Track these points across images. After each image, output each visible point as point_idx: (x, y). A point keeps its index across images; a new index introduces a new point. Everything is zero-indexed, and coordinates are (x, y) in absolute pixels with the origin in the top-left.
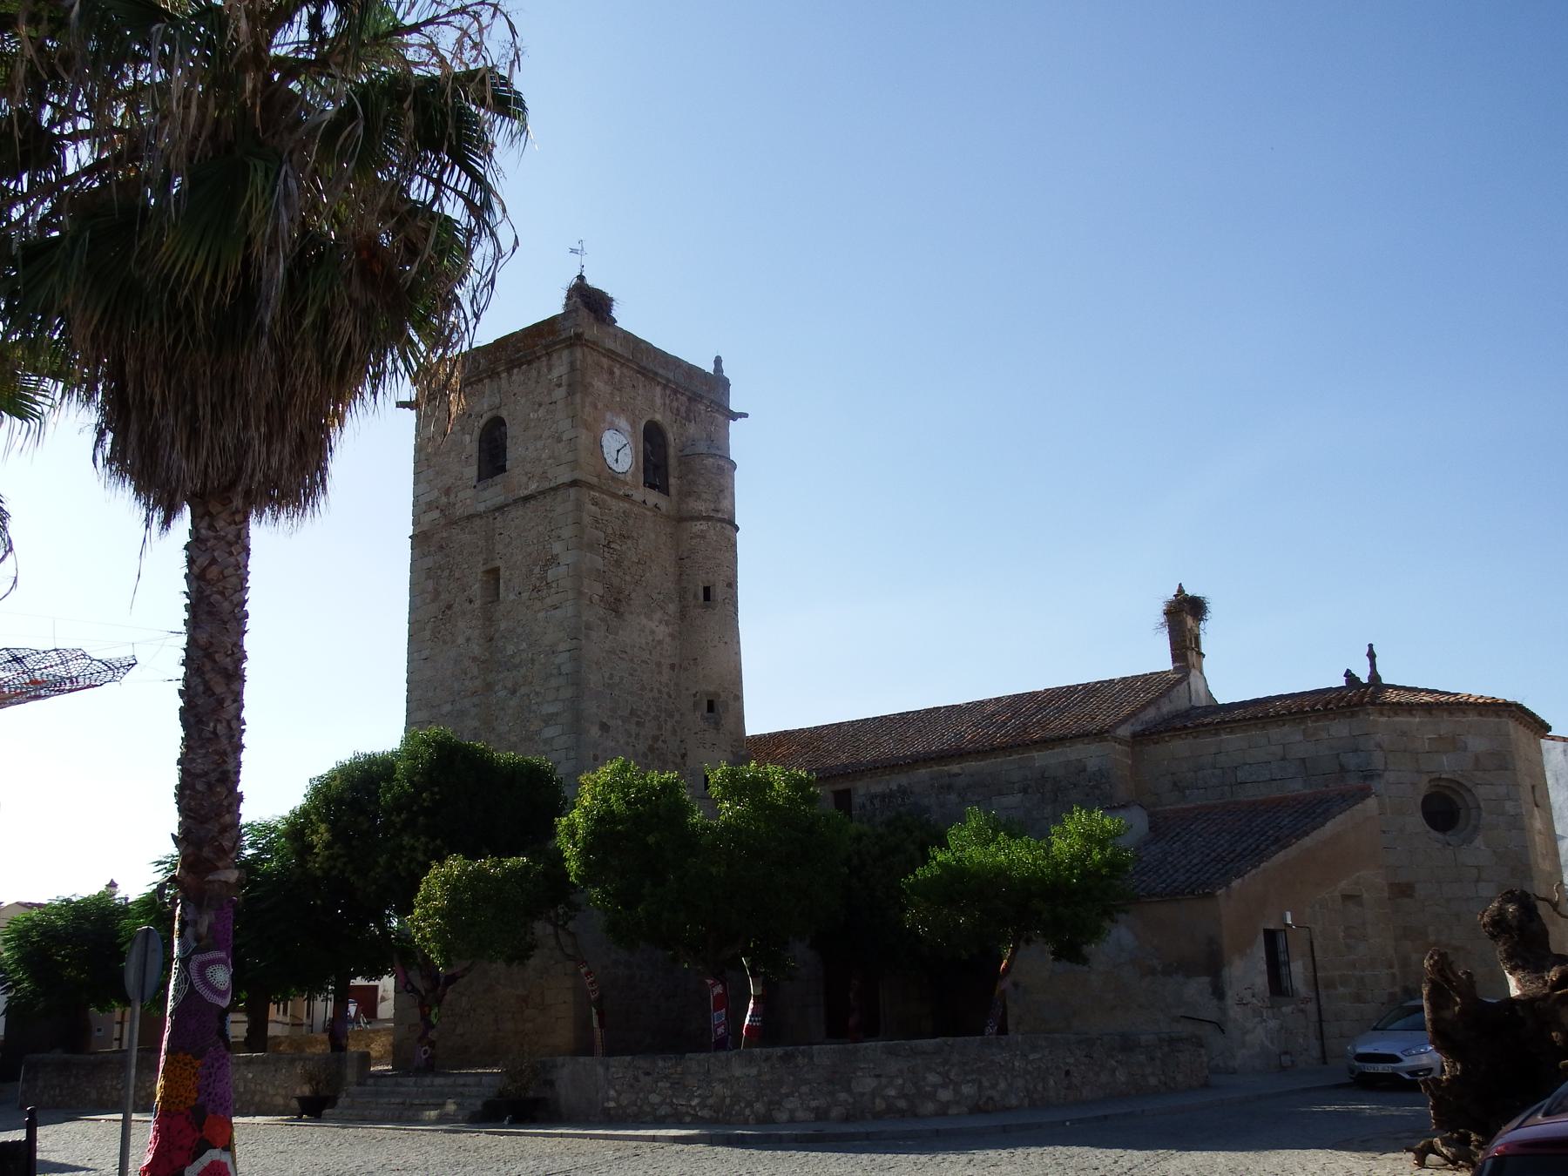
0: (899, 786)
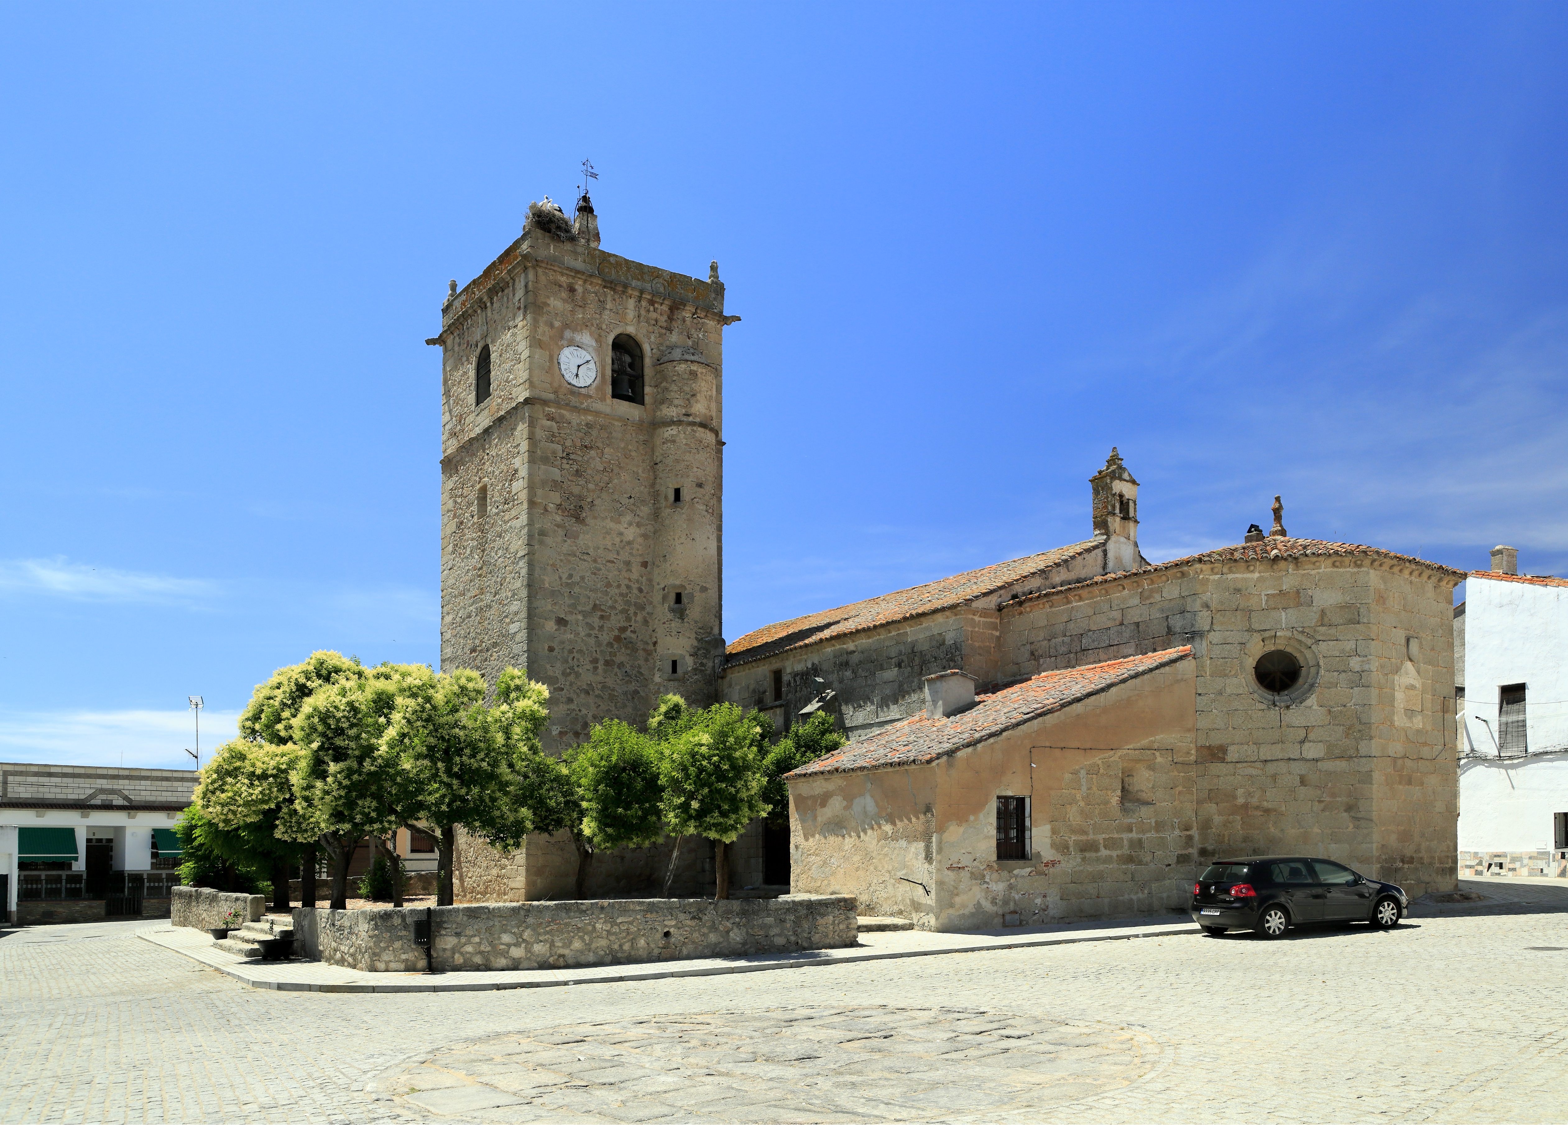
0: (813, 664)
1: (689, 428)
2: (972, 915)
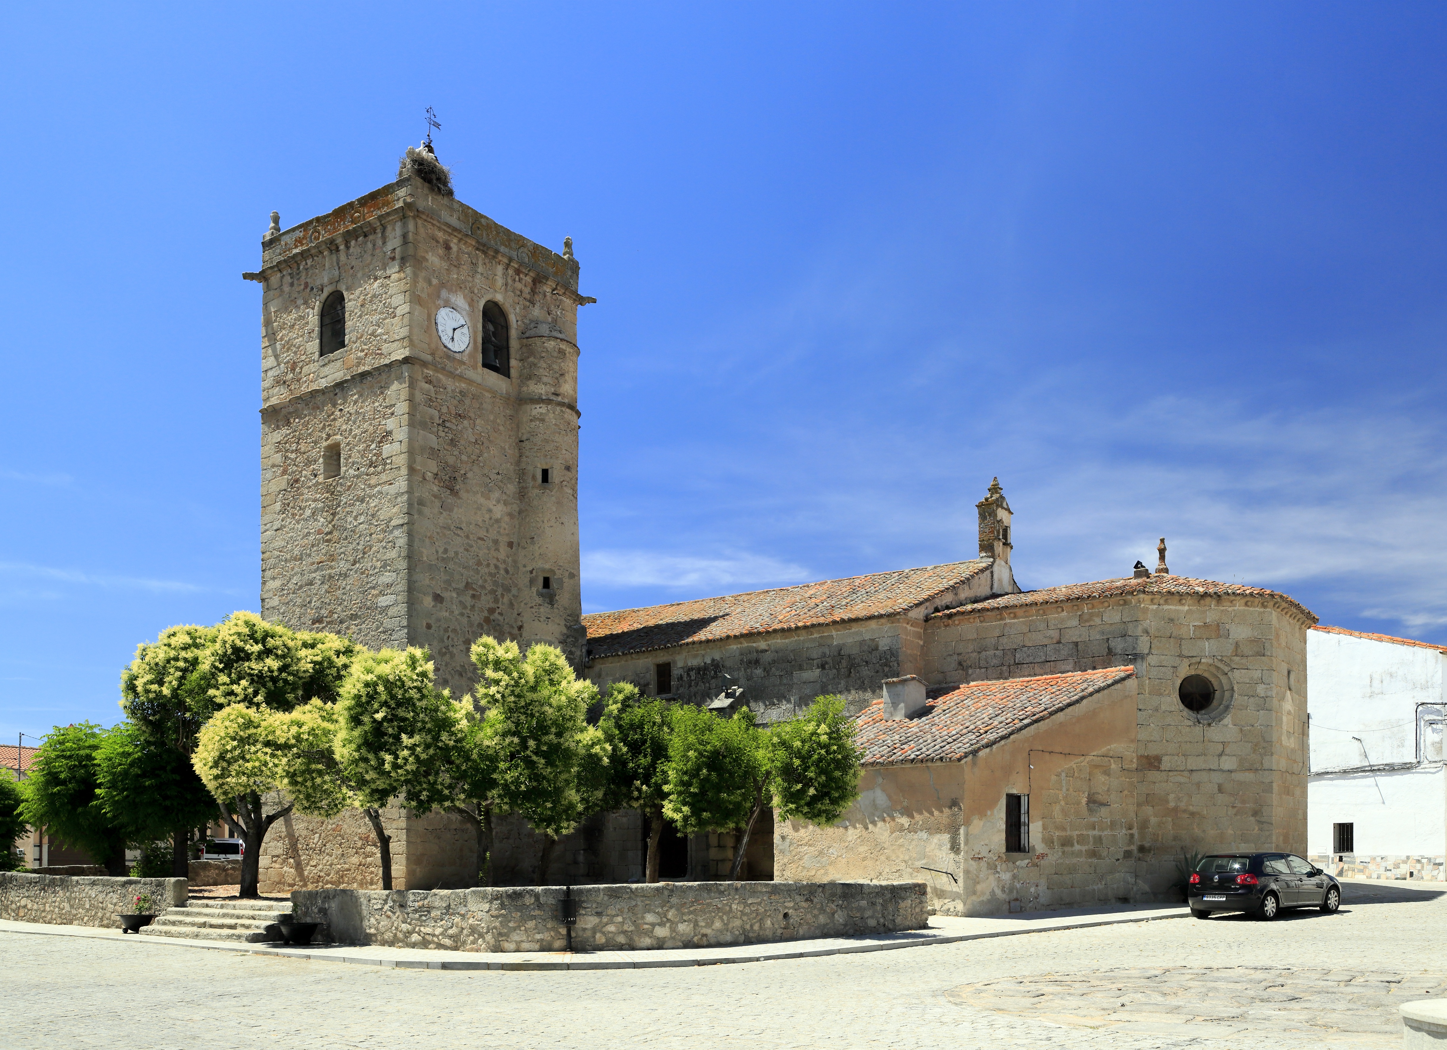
0: (713, 660)
1: (558, 408)
2: (989, 901)
